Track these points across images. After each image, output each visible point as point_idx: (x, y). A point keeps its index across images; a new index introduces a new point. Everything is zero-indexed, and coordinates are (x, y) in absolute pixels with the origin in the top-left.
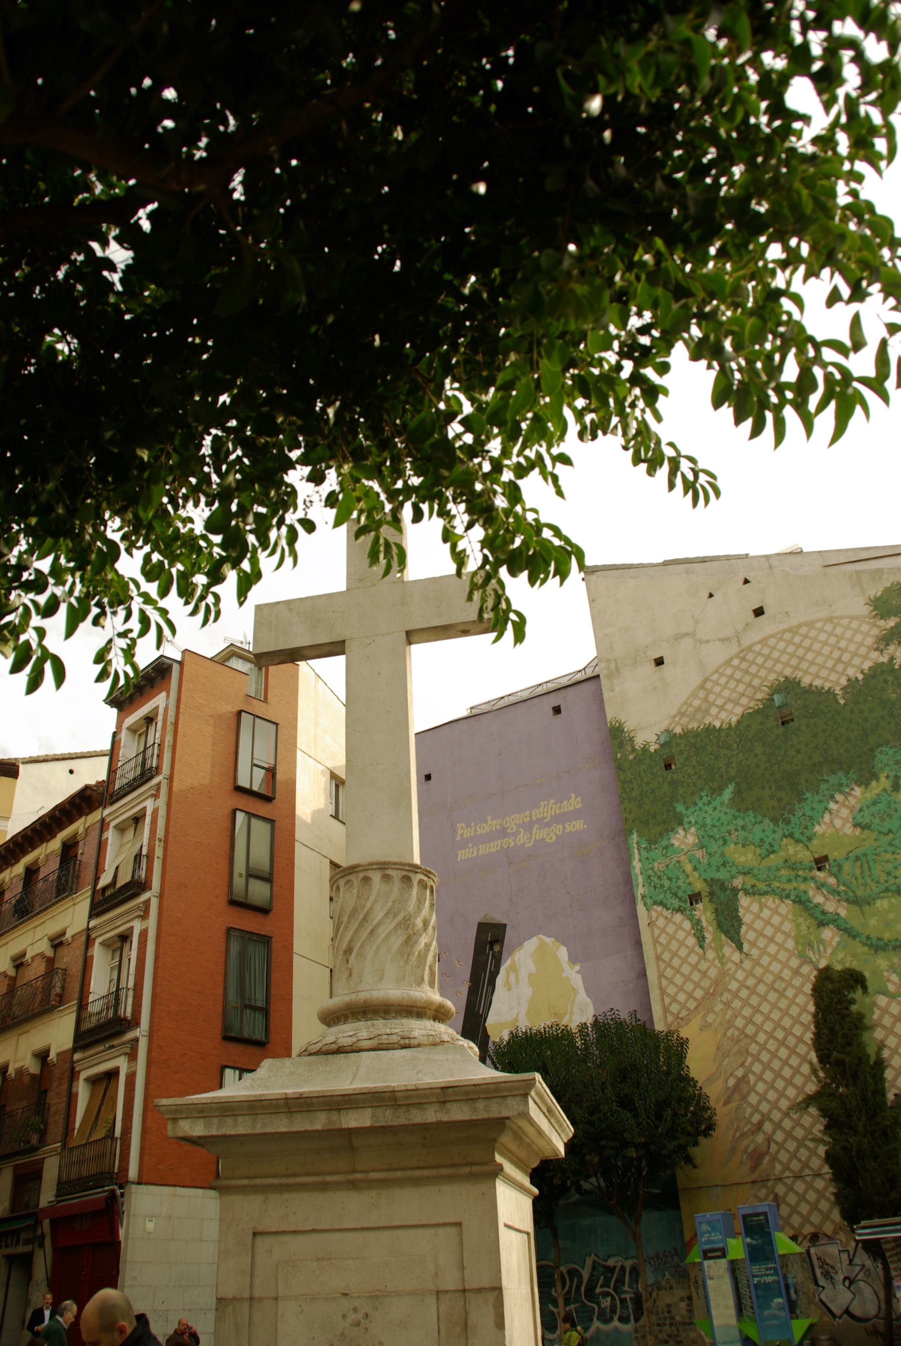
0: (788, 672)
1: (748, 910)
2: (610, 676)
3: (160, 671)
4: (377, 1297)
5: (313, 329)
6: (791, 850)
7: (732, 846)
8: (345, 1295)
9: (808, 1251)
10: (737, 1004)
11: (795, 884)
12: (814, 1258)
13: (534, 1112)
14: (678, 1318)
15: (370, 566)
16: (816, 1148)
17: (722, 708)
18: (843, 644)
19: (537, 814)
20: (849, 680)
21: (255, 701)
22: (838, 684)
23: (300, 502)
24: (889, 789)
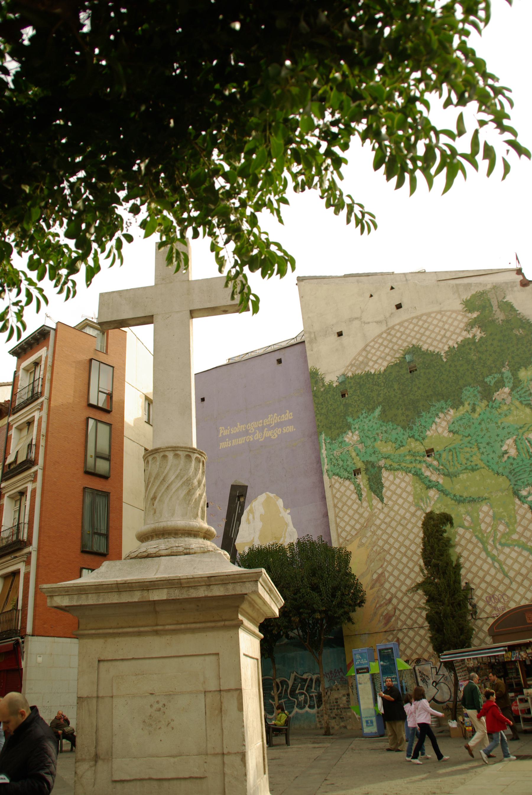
0: (414, 342)
1: (387, 479)
2: (311, 342)
3: (42, 336)
4: (170, 695)
5: (133, 114)
6: (413, 445)
7: (379, 442)
8: (152, 694)
9: (414, 668)
10: (379, 532)
11: (414, 465)
12: (417, 672)
13: (261, 591)
14: (341, 705)
15: (167, 266)
16: (421, 612)
17: (375, 362)
18: (446, 327)
19: (266, 422)
20: (449, 348)
21: (100, 353)
22: (443, 349)
23: (125, 225)
24: (470, 411)
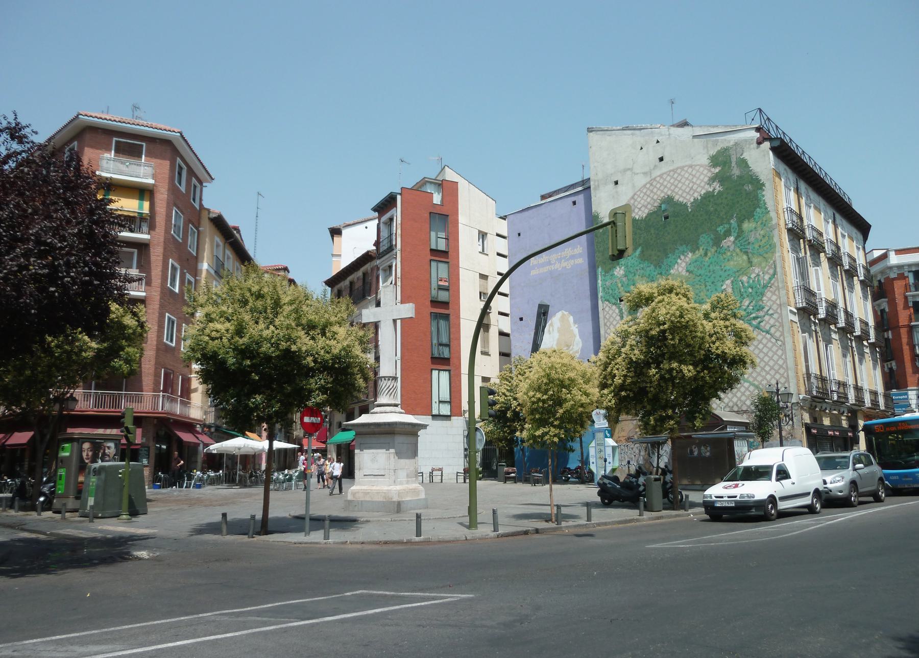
0: (669, 193)
18: (694, 180)
